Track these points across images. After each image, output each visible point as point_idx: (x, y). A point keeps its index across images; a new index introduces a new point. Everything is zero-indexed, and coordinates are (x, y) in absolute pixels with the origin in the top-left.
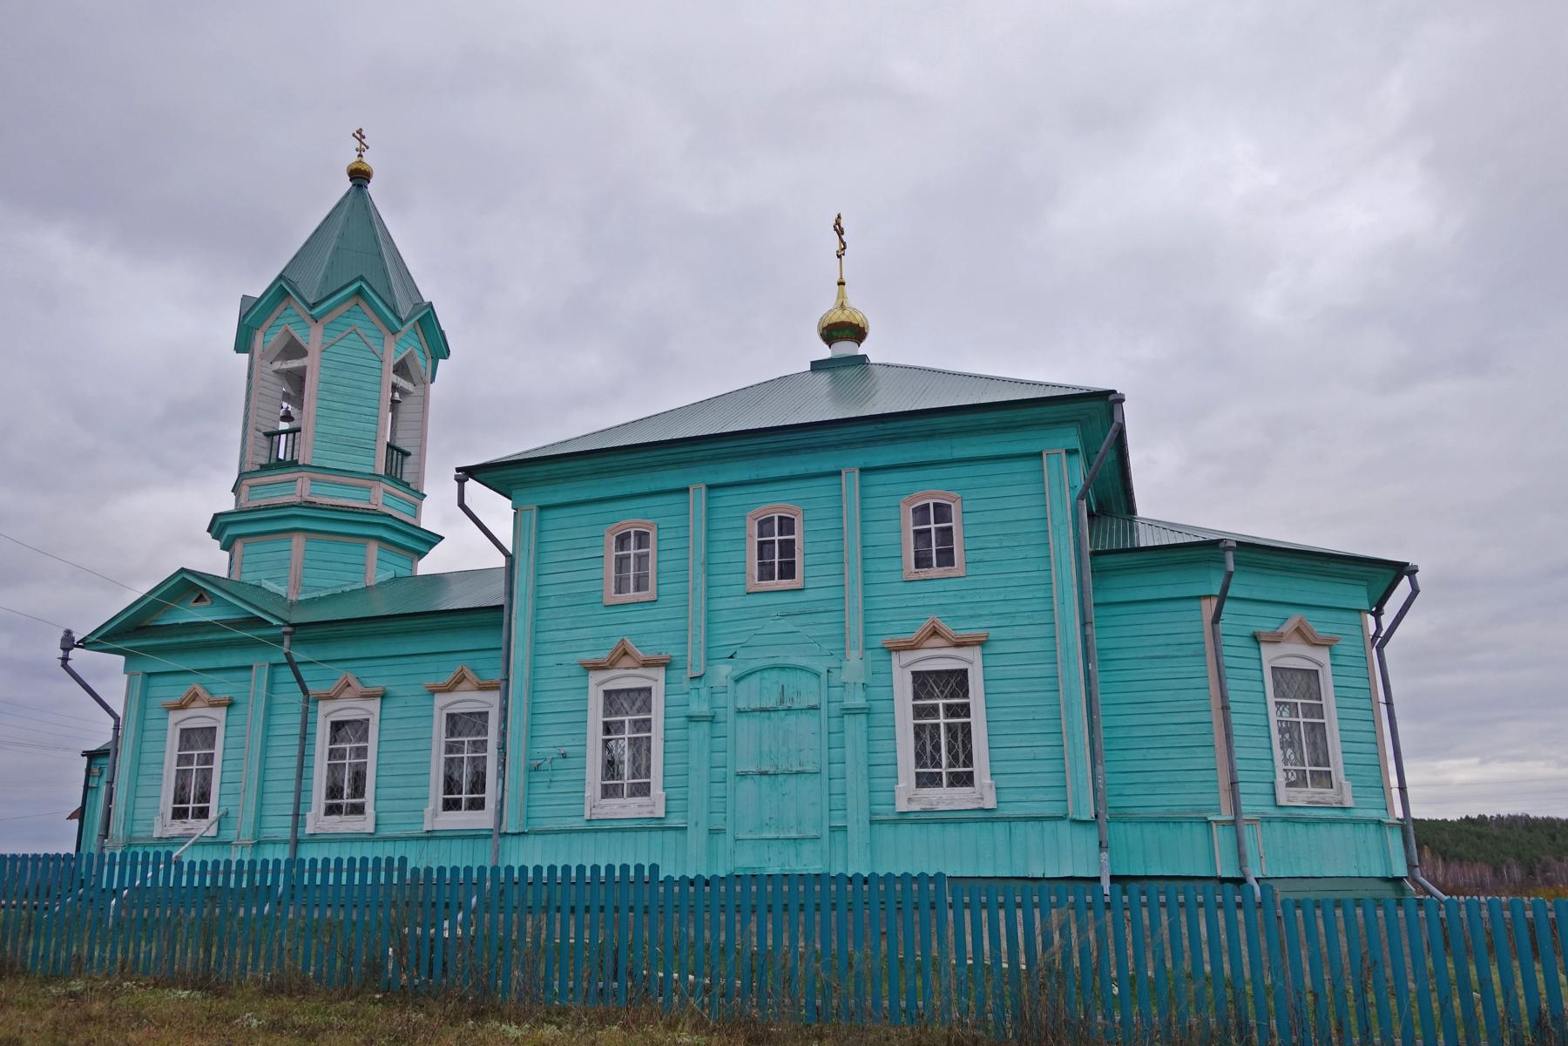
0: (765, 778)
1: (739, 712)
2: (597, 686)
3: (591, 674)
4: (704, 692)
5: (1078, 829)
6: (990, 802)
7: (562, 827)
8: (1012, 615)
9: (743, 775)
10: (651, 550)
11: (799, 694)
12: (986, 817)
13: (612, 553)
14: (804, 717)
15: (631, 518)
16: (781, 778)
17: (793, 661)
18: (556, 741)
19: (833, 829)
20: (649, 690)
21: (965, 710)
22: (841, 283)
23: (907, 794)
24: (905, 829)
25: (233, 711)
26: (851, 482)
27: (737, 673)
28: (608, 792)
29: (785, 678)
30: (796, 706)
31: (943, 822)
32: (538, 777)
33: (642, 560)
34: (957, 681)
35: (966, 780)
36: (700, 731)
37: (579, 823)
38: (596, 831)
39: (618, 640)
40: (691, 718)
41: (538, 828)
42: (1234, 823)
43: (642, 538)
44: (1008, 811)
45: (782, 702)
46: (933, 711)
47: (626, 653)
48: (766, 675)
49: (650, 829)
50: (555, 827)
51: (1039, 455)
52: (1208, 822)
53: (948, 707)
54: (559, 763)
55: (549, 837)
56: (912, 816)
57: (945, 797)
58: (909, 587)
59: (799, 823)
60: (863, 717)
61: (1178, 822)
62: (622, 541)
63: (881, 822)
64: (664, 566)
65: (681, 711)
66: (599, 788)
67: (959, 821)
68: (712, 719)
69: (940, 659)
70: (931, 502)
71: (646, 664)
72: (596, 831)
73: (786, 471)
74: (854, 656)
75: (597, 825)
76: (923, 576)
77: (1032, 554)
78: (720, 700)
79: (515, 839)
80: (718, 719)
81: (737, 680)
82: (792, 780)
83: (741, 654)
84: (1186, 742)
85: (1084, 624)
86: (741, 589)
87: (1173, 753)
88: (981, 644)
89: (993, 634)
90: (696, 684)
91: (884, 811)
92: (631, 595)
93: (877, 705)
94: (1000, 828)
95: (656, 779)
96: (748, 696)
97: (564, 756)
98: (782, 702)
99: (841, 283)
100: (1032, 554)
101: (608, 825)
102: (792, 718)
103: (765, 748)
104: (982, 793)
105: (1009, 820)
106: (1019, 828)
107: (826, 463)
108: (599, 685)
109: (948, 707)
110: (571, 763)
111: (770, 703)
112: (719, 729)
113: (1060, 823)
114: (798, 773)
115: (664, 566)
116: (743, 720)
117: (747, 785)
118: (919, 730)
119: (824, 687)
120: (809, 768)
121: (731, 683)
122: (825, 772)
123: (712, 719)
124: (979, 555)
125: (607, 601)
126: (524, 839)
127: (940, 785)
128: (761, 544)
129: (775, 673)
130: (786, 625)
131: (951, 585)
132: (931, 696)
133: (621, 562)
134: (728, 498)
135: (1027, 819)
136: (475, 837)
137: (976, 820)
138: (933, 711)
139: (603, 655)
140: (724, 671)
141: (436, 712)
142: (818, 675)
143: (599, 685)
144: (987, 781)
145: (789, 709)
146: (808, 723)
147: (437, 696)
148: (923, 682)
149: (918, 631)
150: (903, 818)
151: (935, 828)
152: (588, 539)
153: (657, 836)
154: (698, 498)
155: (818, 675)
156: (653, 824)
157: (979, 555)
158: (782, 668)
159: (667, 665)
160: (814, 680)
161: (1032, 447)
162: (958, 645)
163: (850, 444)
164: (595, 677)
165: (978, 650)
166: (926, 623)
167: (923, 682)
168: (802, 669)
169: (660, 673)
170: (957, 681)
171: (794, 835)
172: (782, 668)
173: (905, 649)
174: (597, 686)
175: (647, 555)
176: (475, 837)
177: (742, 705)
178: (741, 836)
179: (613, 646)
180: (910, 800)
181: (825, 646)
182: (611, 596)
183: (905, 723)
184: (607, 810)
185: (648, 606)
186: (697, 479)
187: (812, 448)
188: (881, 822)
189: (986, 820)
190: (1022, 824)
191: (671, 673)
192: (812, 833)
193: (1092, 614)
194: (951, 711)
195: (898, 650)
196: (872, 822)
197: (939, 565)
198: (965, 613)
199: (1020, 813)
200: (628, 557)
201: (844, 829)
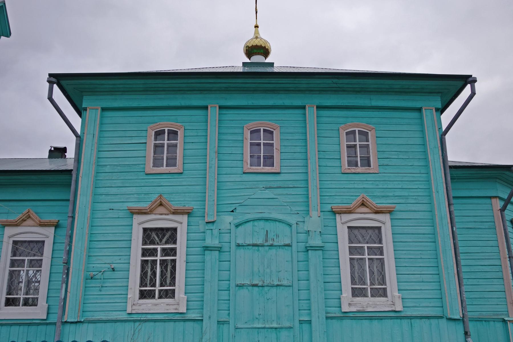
0: (256, 289)
1: (238, 245)
2: (139, 224)
3: (135, 216)
4: (216, 232)
5: (452, 324)
6: (183, 309)
7: (110, 318)
8: (406, 197)
9: (241, 286)
10: (179, 142)
11: (277, 236)
12: (396, 316)
13: (152, 142)
14: (281, 251)
15: (166, 121)
16: (266, 289)
17: (274, 215)
18: (108, 260)
19: (301, 322)
20: (175, 230)
21: (381, 251)
22: (256, 27)
23: (349, 303)
24: (347, 323)
25: (59, 230)
26: (213, 113)
27: (237, 221)
28: (143, 295)
29: (268, 226)
30: (275, 243)
31: (371, 318)
32: (92, 283)
33: (173, 147)
34: (170, 234)
35: (169, 294)
36: (211, 257)
37: (123, 316)
38: (135, 321)
39: (156, 196)
40: (207, 248)
41: (90, 318)
42: (463, 320)
43: (173, 134)
44: (409, 313)
45: (267, 241)
46: (153, 252)
47: (161, 204)
48: (256, 223)
49: (175, 321)
50: (104, 318)
51: (420, 110)
52: (504, 321)
53: (163, 250)
54: (108, 274)
55: (99, 325)
56: (351, 315)
57: (370, 303)
58: (246, 177)
59: (278, 318)
60: (320, 252)
61: (487, 321)
62: (159, 134)
63: (332, 318)
64: (188, 152)
65: (201, 243)
66: (138, 292)
67: (381, 318)
68: (219, 249)
69: (364, 220)
70: (357, 129)
71: (176, 212)
72: (135, 321)
73: (270, 103)
74: (314, 214)
75: (135, 317)
76: (353, 171)
77: (416, 163)
78: (226, 238)
79: (73, 326)
80: (222, 250)
81: (237, 226)
82: (274, 290)
83: (239, 210)
84: (488, 275)
85: (449, 205)
86: (240, 170)
87: (481, 282)
88: (390, 212)
89: (398, 207)
90: (210, 226)
91: (334, 311)
92: (164, 169)
93: (328, 246)
94: (405, 323)
95: (179, 287)
96: (243, 235)
97: (113, 270)
98: (267, 241)
99: (256, 27)
100: (416, 163)
101: (143, 317)
102: (273, 251)
103: (256, 269)
104: (394, 300)
105: (411, 318)
106: (417, 323)
107: (196, 100)
108: (140, 224)
109: (163, 250)
110: (117, 274)
111: (260, 242)
112: (225, 256)
113: (440, 320)
114: (278, 285)
115: (188, 152)
116: (241, 252)
117: (244, 292)
118: (144, 263)
119: (294, 233)
120: (285, 283)
121: (233, 227)
122: (295, 286)
123: (219, 249)
124: (386, 162)
125: (148, 171)
126: (78, 325)
127: (154, 297)
128: (156, 146)
129: (262, 223)
130: (269, 194)
131: (370, 177)
132: (153, 242)
133: (158, 148)
134: (230, 115)
135: (421, 317)
136: (29, 324)
137: (391, 318)
138: (153, 252)
139: (144, 205)
140: (228, 219)
141: (5, 239)
142: (290, 225)
143: (140, 224)
144: (183, 295)
145: (272, 245)
146: (284, 253)
147: (6, 228)
148: (148, 234)
149: (354, 202)
150: (345, 316)
151: (366, 322)
152: (135, 132)
153: (180, 325)
154: (213, 113)
155: (290, 225)
156: (177, 317)
157: (386, 162)
158: (267, 220)
159: (189, 213)
160: (287, 228)
161: (418, 105)
162: (377, 212)
163: (310, 91)
164: (137, 219)
165: (185, 217)
166: (359, 198)
167: (148, 234)
168: (280, 221)
169: (184, 219)
170: (170, 234)
171: (275, 325)
172: (267, 220)
173: (345, 213)
174: (139, 224)
175: (176, 146)
176: (29, 324)
177: (240, 242)
178: (239, 326)
179: (153, 199)
180: (350, 304)
181: (294, 209)
182: (150, 168)
183: (136, 258)
184: (143, 307)
185: (176, 176)
186: (213, 103)
187: (287, 91)
188: (332, 318)
189: (397, 318)
190: (418, 321)
191: (192, 219)
192: (288, 324)
193: (453, 201)
194: (360, 251)
195: (340, 213)
196: (327, 318)
197: (361, 166)
198: (378, 194)
199: (415, 314)
200: (162, 146)
201: (309, 322)
